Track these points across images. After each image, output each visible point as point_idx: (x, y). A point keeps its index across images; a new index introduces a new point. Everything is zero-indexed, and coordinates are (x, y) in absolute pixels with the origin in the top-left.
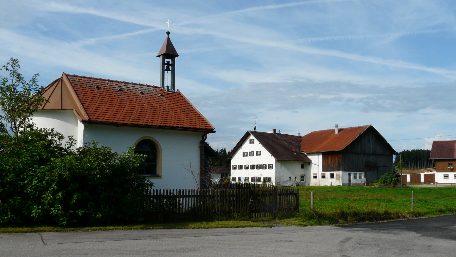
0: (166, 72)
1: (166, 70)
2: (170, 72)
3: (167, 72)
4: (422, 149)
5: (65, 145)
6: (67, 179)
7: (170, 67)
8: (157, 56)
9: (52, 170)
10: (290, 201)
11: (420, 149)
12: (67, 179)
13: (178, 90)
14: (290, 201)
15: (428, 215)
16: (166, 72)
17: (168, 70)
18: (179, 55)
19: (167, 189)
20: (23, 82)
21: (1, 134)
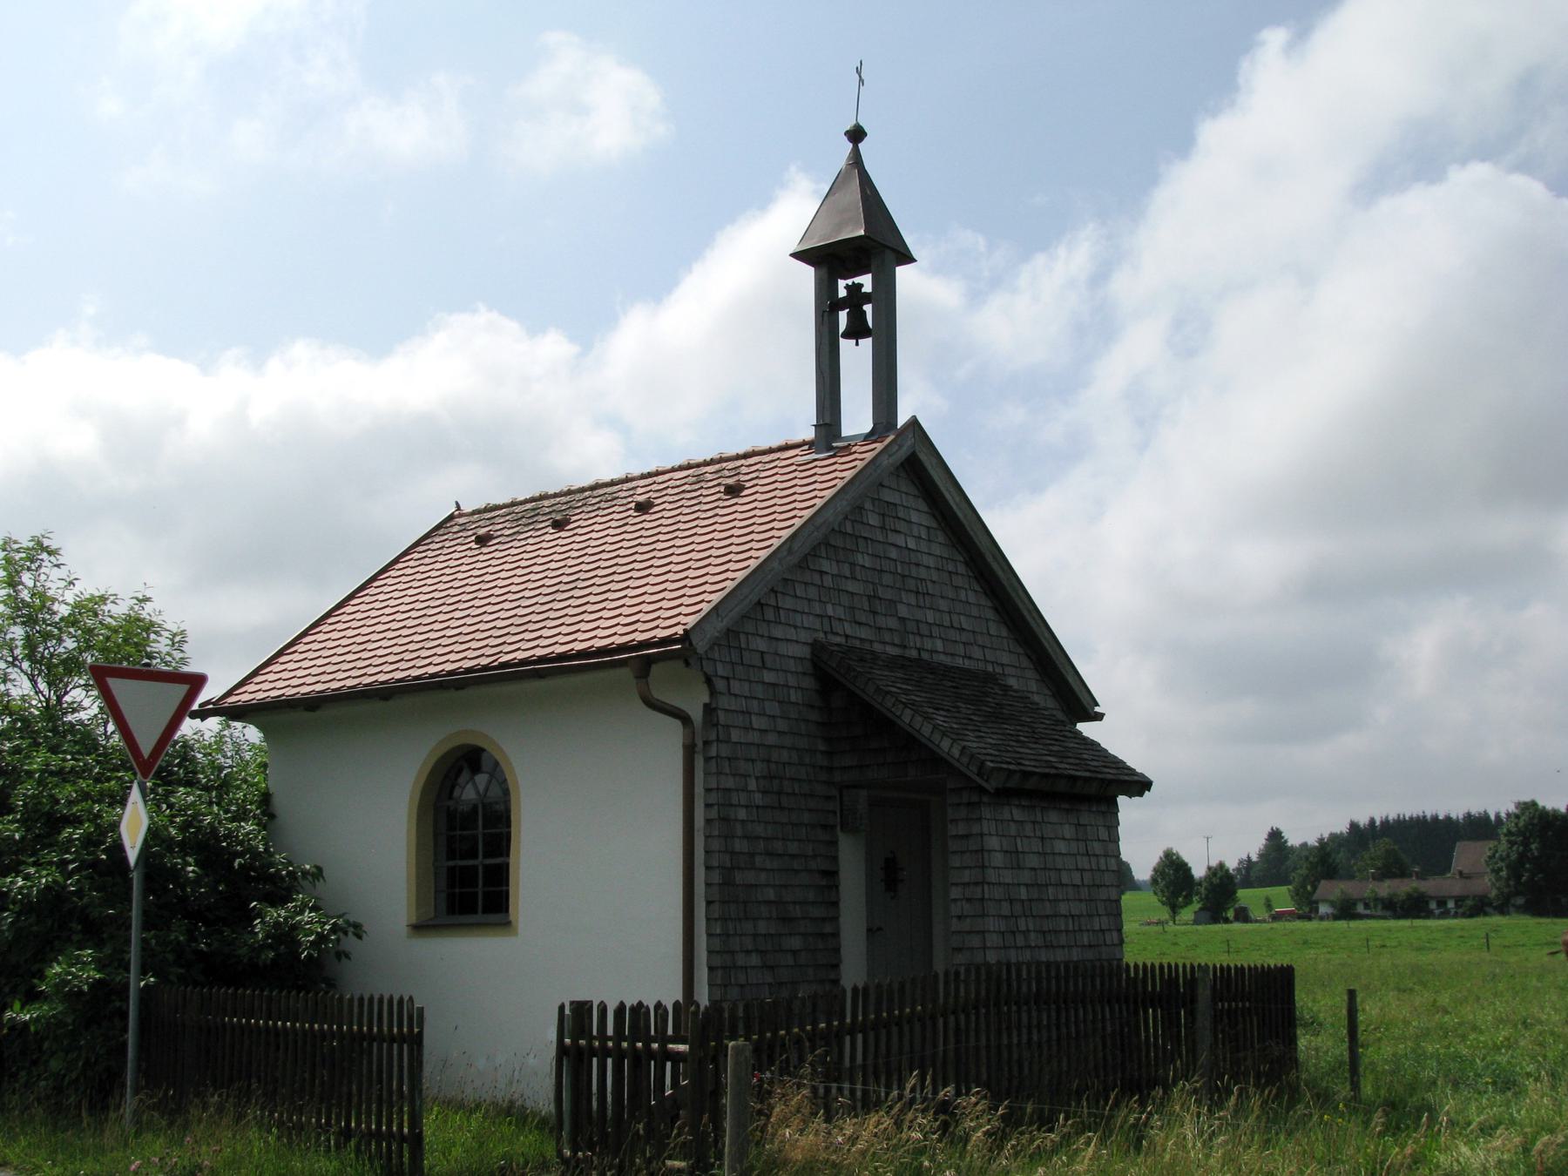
0: (846, 345)
1: (847, 335)
2: (867, 344)
3: (854, 341)
4: (1221, 865)
5: (321, 865)
6: (216, 987)
7: (868, 308)
8: (794, 247)
9: (1389, 1134)
10: (941, 994)
11: (1429, 817)
12: (216, 987)
13: (914, 423)
14: (941, 994)
15: (1200, 990)
16: (846, 345)
17: (857, 330)
18: (915, 257)
19: (659, 1002)
20: (112, 598)
21: (1131, 1175)
